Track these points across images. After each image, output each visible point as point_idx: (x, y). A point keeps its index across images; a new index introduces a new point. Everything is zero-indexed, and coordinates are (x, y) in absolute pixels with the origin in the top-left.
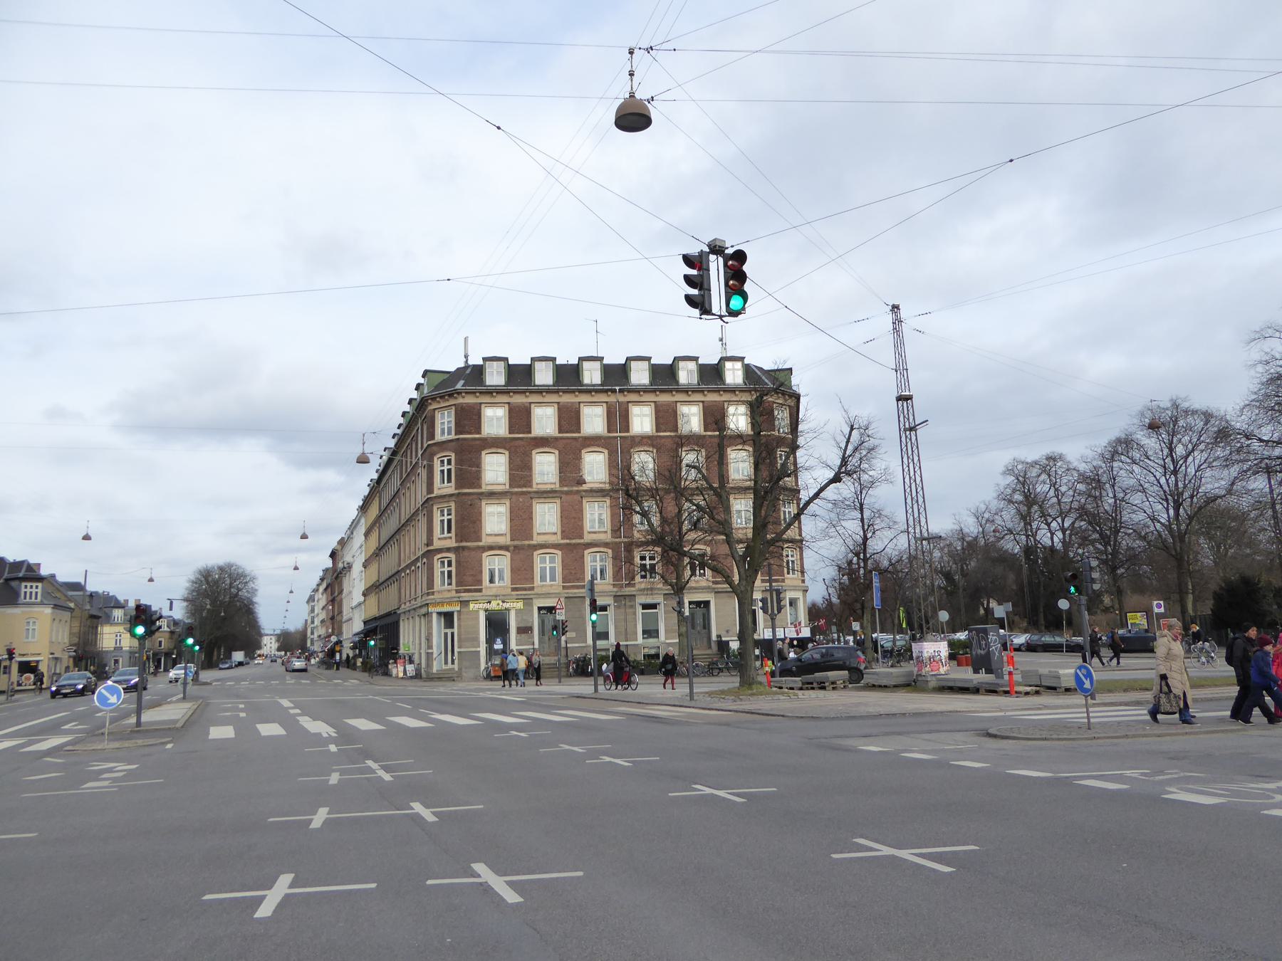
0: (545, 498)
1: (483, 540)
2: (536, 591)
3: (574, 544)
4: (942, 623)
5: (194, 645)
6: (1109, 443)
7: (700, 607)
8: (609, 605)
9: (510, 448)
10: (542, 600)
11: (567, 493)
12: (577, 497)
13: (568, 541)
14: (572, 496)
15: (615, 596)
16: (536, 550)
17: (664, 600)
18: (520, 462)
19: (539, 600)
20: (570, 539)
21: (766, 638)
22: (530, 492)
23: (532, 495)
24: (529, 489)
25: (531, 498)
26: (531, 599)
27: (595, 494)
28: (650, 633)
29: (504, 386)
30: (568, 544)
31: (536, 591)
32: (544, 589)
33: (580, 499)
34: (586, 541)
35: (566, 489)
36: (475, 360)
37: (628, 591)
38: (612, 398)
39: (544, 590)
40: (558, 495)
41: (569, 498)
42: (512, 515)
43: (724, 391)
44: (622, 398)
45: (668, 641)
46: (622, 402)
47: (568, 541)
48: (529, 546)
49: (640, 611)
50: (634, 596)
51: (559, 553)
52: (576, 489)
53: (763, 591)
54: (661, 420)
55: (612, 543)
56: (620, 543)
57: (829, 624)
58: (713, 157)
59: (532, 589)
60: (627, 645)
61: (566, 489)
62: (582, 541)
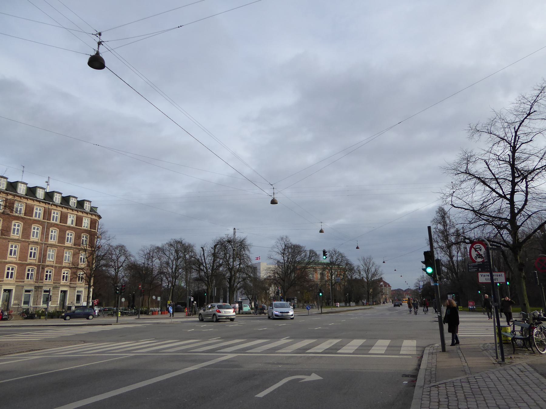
0: (15, 242)
1: (46, 263)
2: (4, 282)
3: (23, 263)
4: (123, 302)
5: (157, 298)
6: (152, 246)
7: (6, 292)
8: (32, 290)
9: (3, 218)
10: (6, 286)
11: (24, 241)
12: (27, 244)
13: (21, 262)
14: (25, 243)
15: (35, 287)
16: (7, 264)
17: (53, 289)
18: (6, 225)
19: (5, 286)
20: (22, 261)
21: (83, 305)
22: (8, 239)
23: (30, 243)
24: (9, 237)
25: (9, 241)
26: (2, 285)
27: (34, 244)
28: (26, 302)
29: (4, 190)
30: (21, 263)
31: (4, 282)
32: (7, 282)
33: (28, 245)
34: (28, 263)
35: (24, 240)
36: (251, 243)
37: (41, 284)
38: (47, 206)
39: (7, 282)
40: (72, 249)
41: (24, 244)
42: (8, 247)
43: (85, 213)
44: (50, 207)
45: (51, 306)
46: (50, 209)
47: (21, 262)
48: (4, 262)
49: (24, 293)
50: (42, 287)
51: (16, 266)
52: (28, 240)
53: (85, 288)
54: (62, 219)
55: (37, 265)
56: (41, 265)
57: (165, 300)
58: (162, 161)
59: (76, 284)
60: (36, 307)
61: (24, 240)
62: (26, 262)
